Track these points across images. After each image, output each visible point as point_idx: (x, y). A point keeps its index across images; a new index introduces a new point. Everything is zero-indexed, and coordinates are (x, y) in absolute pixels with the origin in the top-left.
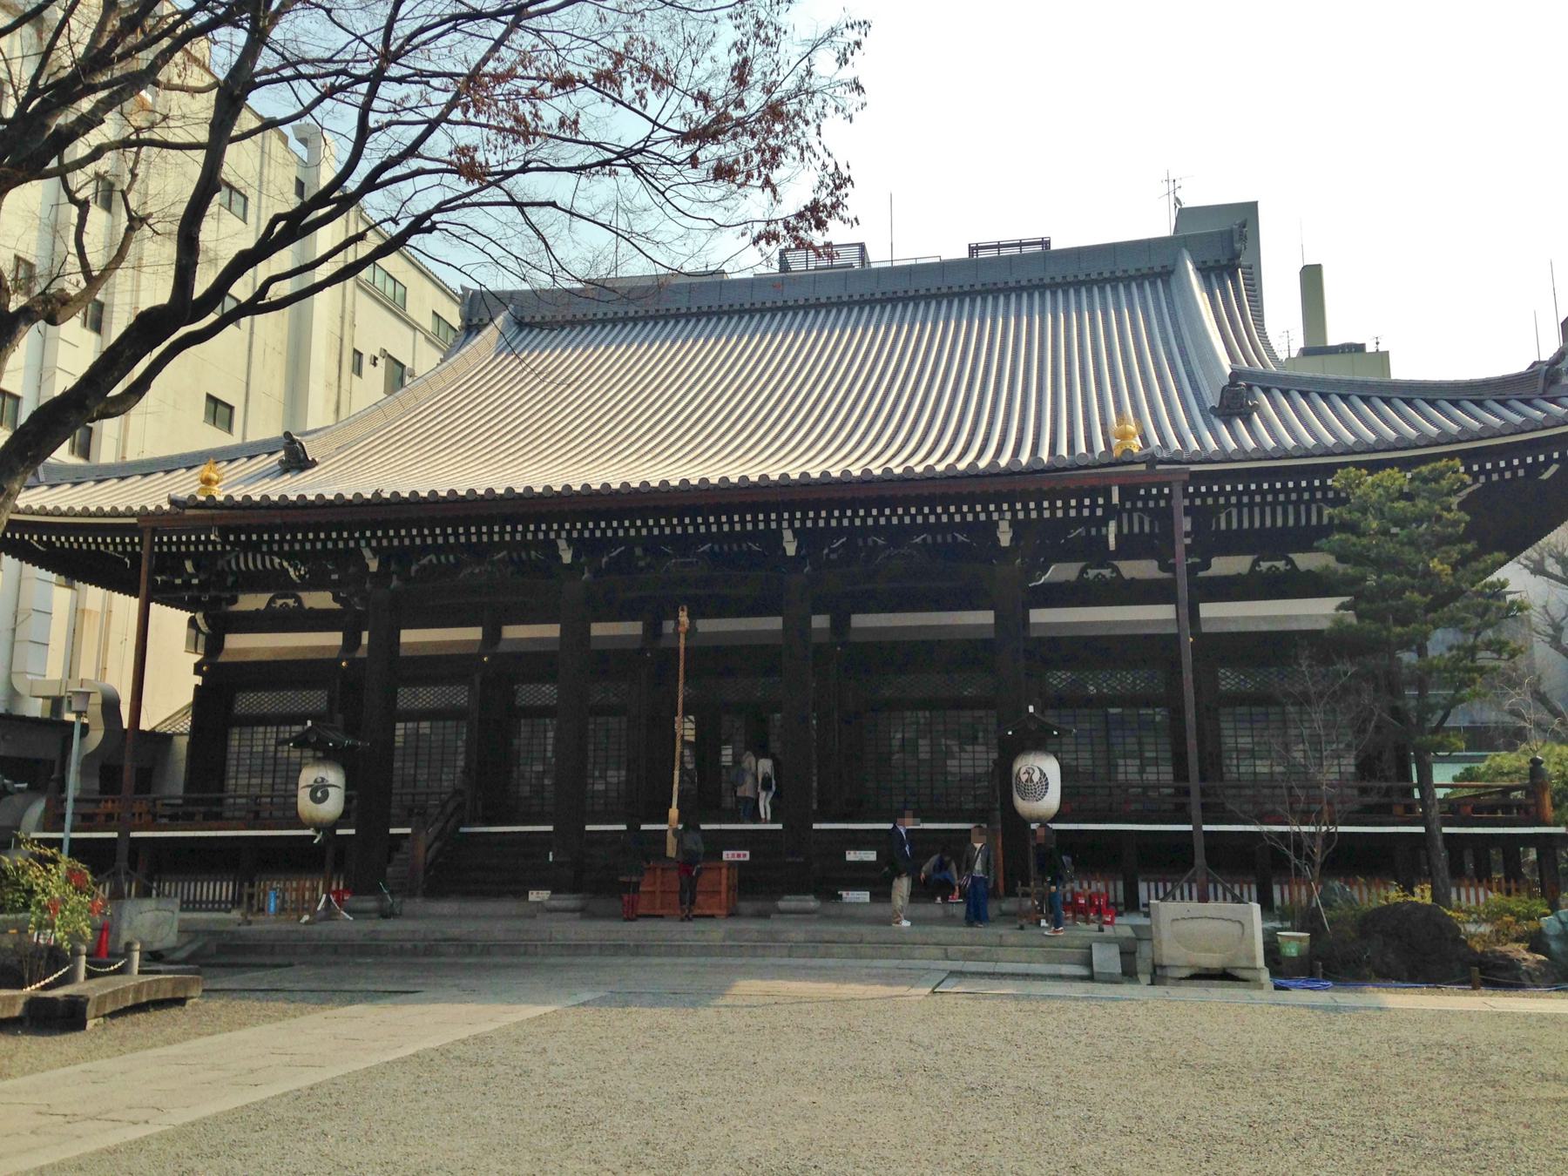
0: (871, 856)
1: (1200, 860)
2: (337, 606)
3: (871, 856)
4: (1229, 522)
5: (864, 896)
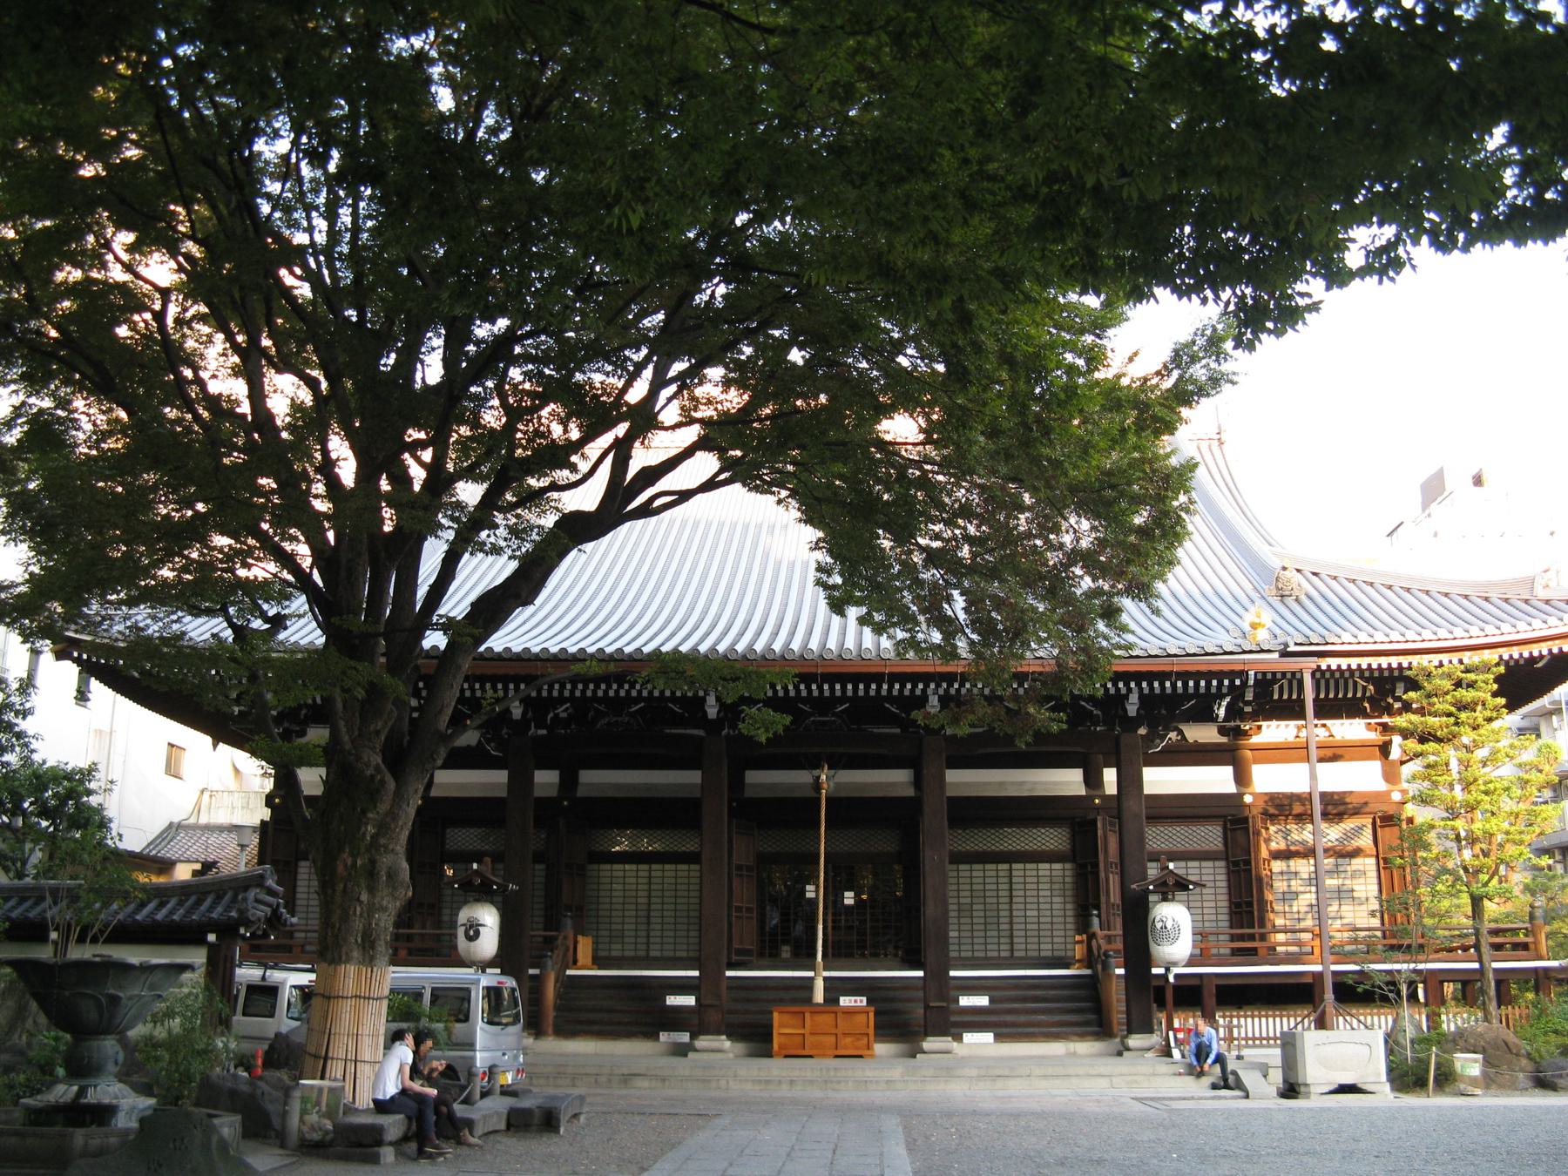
0: (983, 1001)
1: (1329, 996)
2: (1224, 740)
3: (983, 1001)
4: (1281, 694)
5: (988, 1037)
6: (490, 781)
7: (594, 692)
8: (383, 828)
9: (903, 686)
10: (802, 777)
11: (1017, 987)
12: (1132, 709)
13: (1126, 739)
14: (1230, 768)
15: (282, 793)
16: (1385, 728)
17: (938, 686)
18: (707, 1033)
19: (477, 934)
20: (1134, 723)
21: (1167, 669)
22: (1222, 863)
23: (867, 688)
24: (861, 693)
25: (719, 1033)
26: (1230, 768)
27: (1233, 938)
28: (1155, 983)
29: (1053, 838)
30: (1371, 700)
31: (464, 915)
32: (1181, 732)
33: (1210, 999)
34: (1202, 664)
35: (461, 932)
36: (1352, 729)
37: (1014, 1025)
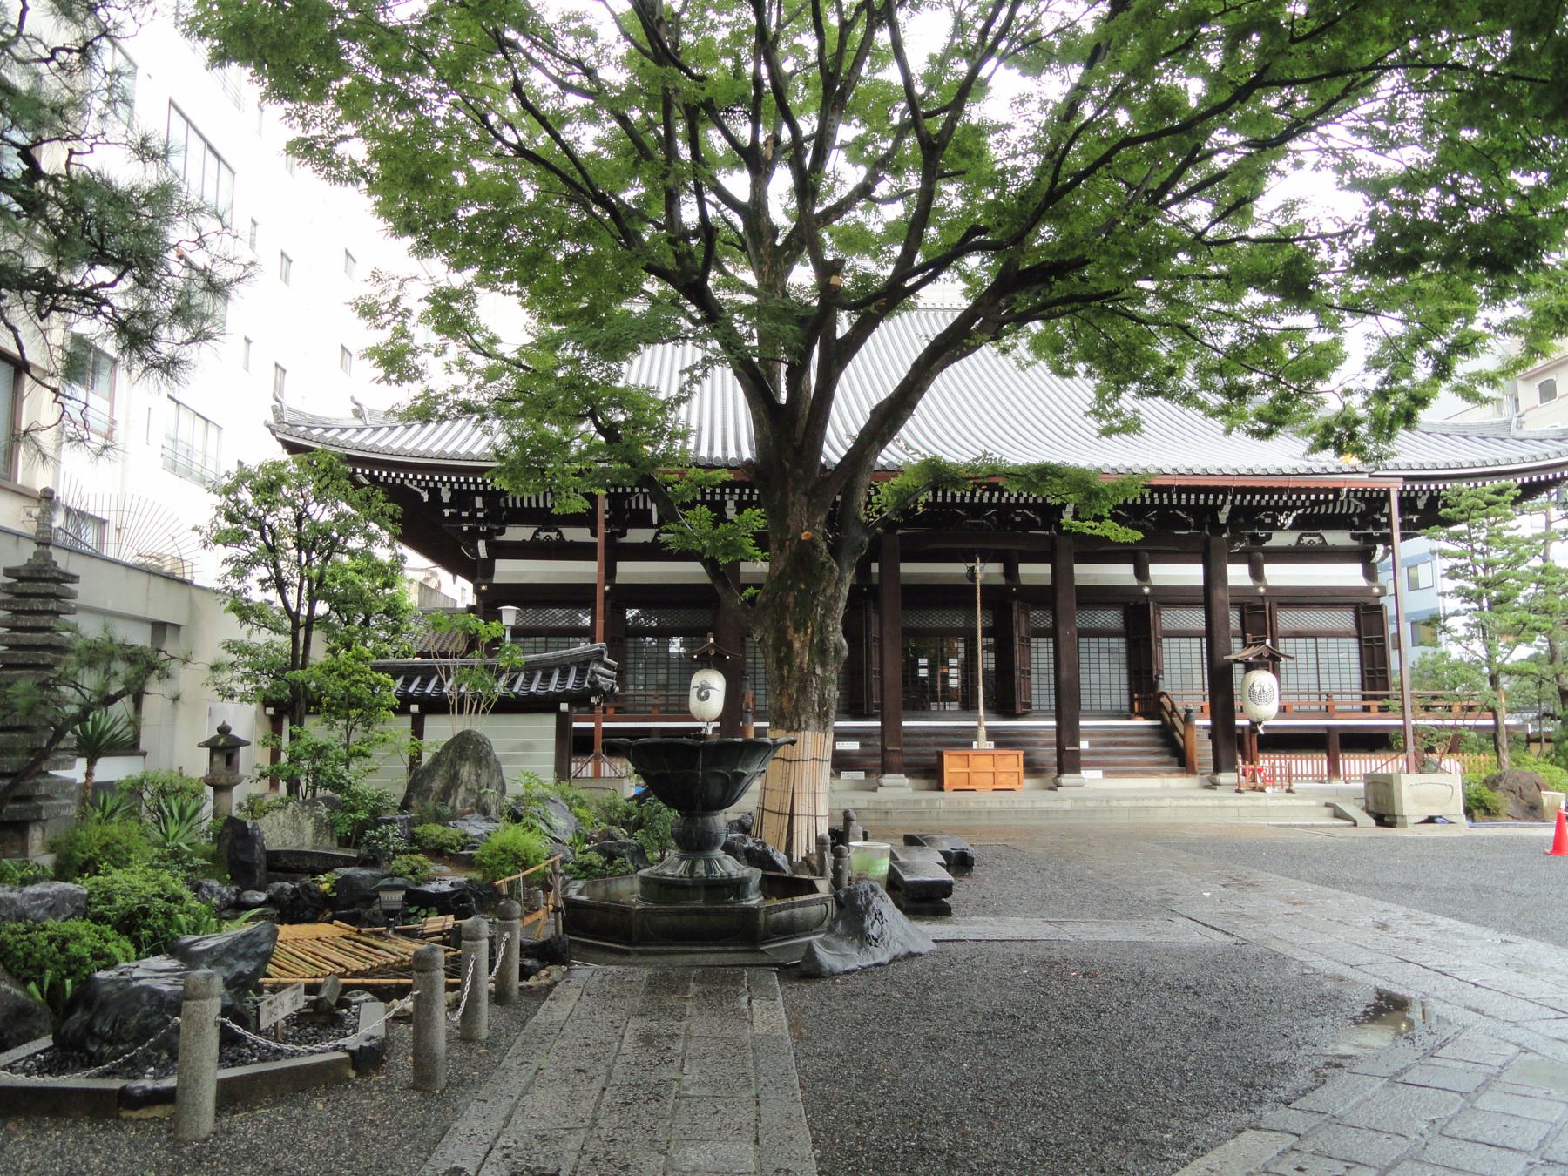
5: (1097, 774)
6: (1089, 573)
7: (750, 496)
8: (829, 609)
9: (1244, 497)
10: (960, 569)
11: (1109, 735)
12: (1223, 517)
13: (1214, 540)
14: (1246, 567)
15: (479, 580)
16: (1368, 538)
17: (732, 493)
18: (891, 772)
19: (707, 697)
20: (1222, 528)
21: (1284, 485)
22: (1122, 640)
23: (1207, 498)
24: (1192, 502)
25: (900, 772)
26: (1246, 567)
27: (1364, 698)
28: (1239, 731)
29: (1111, 618)
30: (1361, 516)
31: (697, 679)
32: (560, 533)
33: (1335, 741)
34: (1292, 483)
35: (693, 693)
36: (1339, 538)
37: (1115, 764)
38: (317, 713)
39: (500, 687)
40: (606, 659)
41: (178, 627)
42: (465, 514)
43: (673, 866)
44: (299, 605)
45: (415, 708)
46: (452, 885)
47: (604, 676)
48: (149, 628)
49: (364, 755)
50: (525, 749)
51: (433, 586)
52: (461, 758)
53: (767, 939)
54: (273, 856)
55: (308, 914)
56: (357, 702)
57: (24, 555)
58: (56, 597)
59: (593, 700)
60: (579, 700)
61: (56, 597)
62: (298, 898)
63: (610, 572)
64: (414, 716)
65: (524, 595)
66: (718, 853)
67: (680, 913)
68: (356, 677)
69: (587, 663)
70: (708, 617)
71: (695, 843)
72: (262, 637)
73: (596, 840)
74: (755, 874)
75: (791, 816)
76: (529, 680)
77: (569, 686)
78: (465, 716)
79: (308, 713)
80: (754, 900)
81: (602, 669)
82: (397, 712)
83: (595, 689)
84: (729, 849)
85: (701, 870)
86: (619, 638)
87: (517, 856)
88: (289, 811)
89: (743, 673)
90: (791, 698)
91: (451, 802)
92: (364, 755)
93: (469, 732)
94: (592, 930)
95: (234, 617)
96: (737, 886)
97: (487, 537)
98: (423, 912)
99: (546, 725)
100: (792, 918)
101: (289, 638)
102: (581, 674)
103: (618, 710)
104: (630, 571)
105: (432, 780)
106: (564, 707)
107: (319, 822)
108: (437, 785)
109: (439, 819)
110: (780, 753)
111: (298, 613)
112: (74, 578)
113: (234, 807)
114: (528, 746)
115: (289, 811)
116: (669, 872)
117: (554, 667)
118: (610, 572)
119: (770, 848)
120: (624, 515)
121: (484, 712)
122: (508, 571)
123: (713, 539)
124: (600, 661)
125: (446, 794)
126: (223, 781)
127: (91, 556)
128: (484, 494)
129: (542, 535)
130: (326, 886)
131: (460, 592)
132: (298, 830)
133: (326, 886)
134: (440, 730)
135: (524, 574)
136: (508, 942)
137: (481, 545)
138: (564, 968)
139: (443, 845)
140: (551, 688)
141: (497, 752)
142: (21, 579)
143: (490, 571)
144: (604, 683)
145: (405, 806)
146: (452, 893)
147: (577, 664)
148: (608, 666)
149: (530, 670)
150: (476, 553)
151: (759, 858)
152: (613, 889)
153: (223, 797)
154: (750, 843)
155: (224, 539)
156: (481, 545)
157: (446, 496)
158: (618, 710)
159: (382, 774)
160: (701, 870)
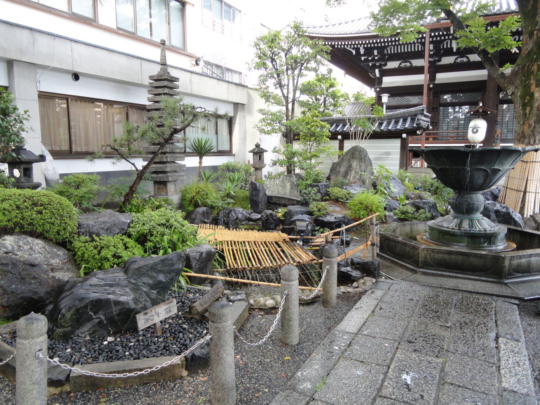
15: (376, 86)
31: (472, 124)
35: (470, 131)
38: (299, 139)
39: (375, 127)
40: (425, 113)
41: (244, 105)
42: (370, 58)
43: (449, 223)
44: (288, 93)
45: (340, 137)
46: (335, 218)
47: (424, 121)
48: (232, 106)
49: (316, 156)
50: (386, 156)
51: (348, 85)
52: (353, 158)
53: (510, 275)
54: (270, 198)
55: (272, 226)
56: (313, 135)
57: (156, 70)
58: (171, 88)
59: (418, 132)
60: (412, 132)
61: (171, 88)
62: (268, 219)
63: (432, 78)
64: (340, 140)
65: (394, 92)
66: (478, 215)
67: (450, 253)
68: (313, 124)
69: (416, 115)
70: (480, 97)
71: (464, 209)
72: (275, 108)
73: (412, 198)
74: (502, 229)
75: (525, 192)
76: (389, 124)
77: (407, 126)
78: (357, 140)
79: (294, 139)
80: (500, 246)
81: (423, 118)
82: (331, 139)
83: (419, 127)
84: (486, 213)
85: (466, 225)
86: (436, 107)
87: (367, 207)
88: (281, 179)
89: (496, 121)
90: (530, 126)
91: (348, 177)
92: (316, 156)
93: (356, 147)
94: (396, 253)
95: (263, 100)
96: (490, 238)
97: (380, 67)
98: (321, 230)
99: (395, 145)
100: (529, 264)
101: (285, 107)
102: (413, 120)
103: (434, 139)
104: (442, 77)
105: (340, 168)
106: (404, 136)
107: (292, 184)
108: (342, 169)
109: (342, 185)
110: (526, 157)
111: (287, 97)
112: (177, 79)
113: (263, 177)
114: (388, 154)
115: (281, 179)
116: (445, 225)
117: (400, 118)
118: (432, 78)
119: (511, 210)
120: (440, 51)
121: (366, 138)
122: (388, 81)
123: (486, 38)
124: (422, 114)
125: (346, 174)
126: (257, 166)
127: (236, 84)
128: (377, 48)
129: (403, 65)
130: (280, 215)
131: (370, 93)
132: (284, 187)
133: (280, 215)
134: (348, 145)
135: (395, 82)
136: (328, 270)
137: (377, 71)
138: (374, 280)
139: (338, 198)
140: (398, 127)
141: (371, 156)
142: (156, 80)
143: (380, 82)
144: (424, 124)
145: (329, 178)
146: (335, 222)
147: (411, 116)
148: (426, 116)
149: (389, 119)
150: (375, 75)
151: (504, 218)
152: (415, 228)
153: (258, 172)
154: (498, 207)
155: (258, 66)
156: (377, 71)
157: (362, 51)
158: (434, 139)
159: (322, 166)
160: (466, 225)
